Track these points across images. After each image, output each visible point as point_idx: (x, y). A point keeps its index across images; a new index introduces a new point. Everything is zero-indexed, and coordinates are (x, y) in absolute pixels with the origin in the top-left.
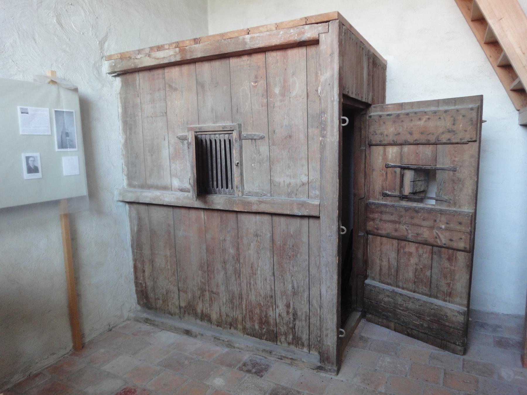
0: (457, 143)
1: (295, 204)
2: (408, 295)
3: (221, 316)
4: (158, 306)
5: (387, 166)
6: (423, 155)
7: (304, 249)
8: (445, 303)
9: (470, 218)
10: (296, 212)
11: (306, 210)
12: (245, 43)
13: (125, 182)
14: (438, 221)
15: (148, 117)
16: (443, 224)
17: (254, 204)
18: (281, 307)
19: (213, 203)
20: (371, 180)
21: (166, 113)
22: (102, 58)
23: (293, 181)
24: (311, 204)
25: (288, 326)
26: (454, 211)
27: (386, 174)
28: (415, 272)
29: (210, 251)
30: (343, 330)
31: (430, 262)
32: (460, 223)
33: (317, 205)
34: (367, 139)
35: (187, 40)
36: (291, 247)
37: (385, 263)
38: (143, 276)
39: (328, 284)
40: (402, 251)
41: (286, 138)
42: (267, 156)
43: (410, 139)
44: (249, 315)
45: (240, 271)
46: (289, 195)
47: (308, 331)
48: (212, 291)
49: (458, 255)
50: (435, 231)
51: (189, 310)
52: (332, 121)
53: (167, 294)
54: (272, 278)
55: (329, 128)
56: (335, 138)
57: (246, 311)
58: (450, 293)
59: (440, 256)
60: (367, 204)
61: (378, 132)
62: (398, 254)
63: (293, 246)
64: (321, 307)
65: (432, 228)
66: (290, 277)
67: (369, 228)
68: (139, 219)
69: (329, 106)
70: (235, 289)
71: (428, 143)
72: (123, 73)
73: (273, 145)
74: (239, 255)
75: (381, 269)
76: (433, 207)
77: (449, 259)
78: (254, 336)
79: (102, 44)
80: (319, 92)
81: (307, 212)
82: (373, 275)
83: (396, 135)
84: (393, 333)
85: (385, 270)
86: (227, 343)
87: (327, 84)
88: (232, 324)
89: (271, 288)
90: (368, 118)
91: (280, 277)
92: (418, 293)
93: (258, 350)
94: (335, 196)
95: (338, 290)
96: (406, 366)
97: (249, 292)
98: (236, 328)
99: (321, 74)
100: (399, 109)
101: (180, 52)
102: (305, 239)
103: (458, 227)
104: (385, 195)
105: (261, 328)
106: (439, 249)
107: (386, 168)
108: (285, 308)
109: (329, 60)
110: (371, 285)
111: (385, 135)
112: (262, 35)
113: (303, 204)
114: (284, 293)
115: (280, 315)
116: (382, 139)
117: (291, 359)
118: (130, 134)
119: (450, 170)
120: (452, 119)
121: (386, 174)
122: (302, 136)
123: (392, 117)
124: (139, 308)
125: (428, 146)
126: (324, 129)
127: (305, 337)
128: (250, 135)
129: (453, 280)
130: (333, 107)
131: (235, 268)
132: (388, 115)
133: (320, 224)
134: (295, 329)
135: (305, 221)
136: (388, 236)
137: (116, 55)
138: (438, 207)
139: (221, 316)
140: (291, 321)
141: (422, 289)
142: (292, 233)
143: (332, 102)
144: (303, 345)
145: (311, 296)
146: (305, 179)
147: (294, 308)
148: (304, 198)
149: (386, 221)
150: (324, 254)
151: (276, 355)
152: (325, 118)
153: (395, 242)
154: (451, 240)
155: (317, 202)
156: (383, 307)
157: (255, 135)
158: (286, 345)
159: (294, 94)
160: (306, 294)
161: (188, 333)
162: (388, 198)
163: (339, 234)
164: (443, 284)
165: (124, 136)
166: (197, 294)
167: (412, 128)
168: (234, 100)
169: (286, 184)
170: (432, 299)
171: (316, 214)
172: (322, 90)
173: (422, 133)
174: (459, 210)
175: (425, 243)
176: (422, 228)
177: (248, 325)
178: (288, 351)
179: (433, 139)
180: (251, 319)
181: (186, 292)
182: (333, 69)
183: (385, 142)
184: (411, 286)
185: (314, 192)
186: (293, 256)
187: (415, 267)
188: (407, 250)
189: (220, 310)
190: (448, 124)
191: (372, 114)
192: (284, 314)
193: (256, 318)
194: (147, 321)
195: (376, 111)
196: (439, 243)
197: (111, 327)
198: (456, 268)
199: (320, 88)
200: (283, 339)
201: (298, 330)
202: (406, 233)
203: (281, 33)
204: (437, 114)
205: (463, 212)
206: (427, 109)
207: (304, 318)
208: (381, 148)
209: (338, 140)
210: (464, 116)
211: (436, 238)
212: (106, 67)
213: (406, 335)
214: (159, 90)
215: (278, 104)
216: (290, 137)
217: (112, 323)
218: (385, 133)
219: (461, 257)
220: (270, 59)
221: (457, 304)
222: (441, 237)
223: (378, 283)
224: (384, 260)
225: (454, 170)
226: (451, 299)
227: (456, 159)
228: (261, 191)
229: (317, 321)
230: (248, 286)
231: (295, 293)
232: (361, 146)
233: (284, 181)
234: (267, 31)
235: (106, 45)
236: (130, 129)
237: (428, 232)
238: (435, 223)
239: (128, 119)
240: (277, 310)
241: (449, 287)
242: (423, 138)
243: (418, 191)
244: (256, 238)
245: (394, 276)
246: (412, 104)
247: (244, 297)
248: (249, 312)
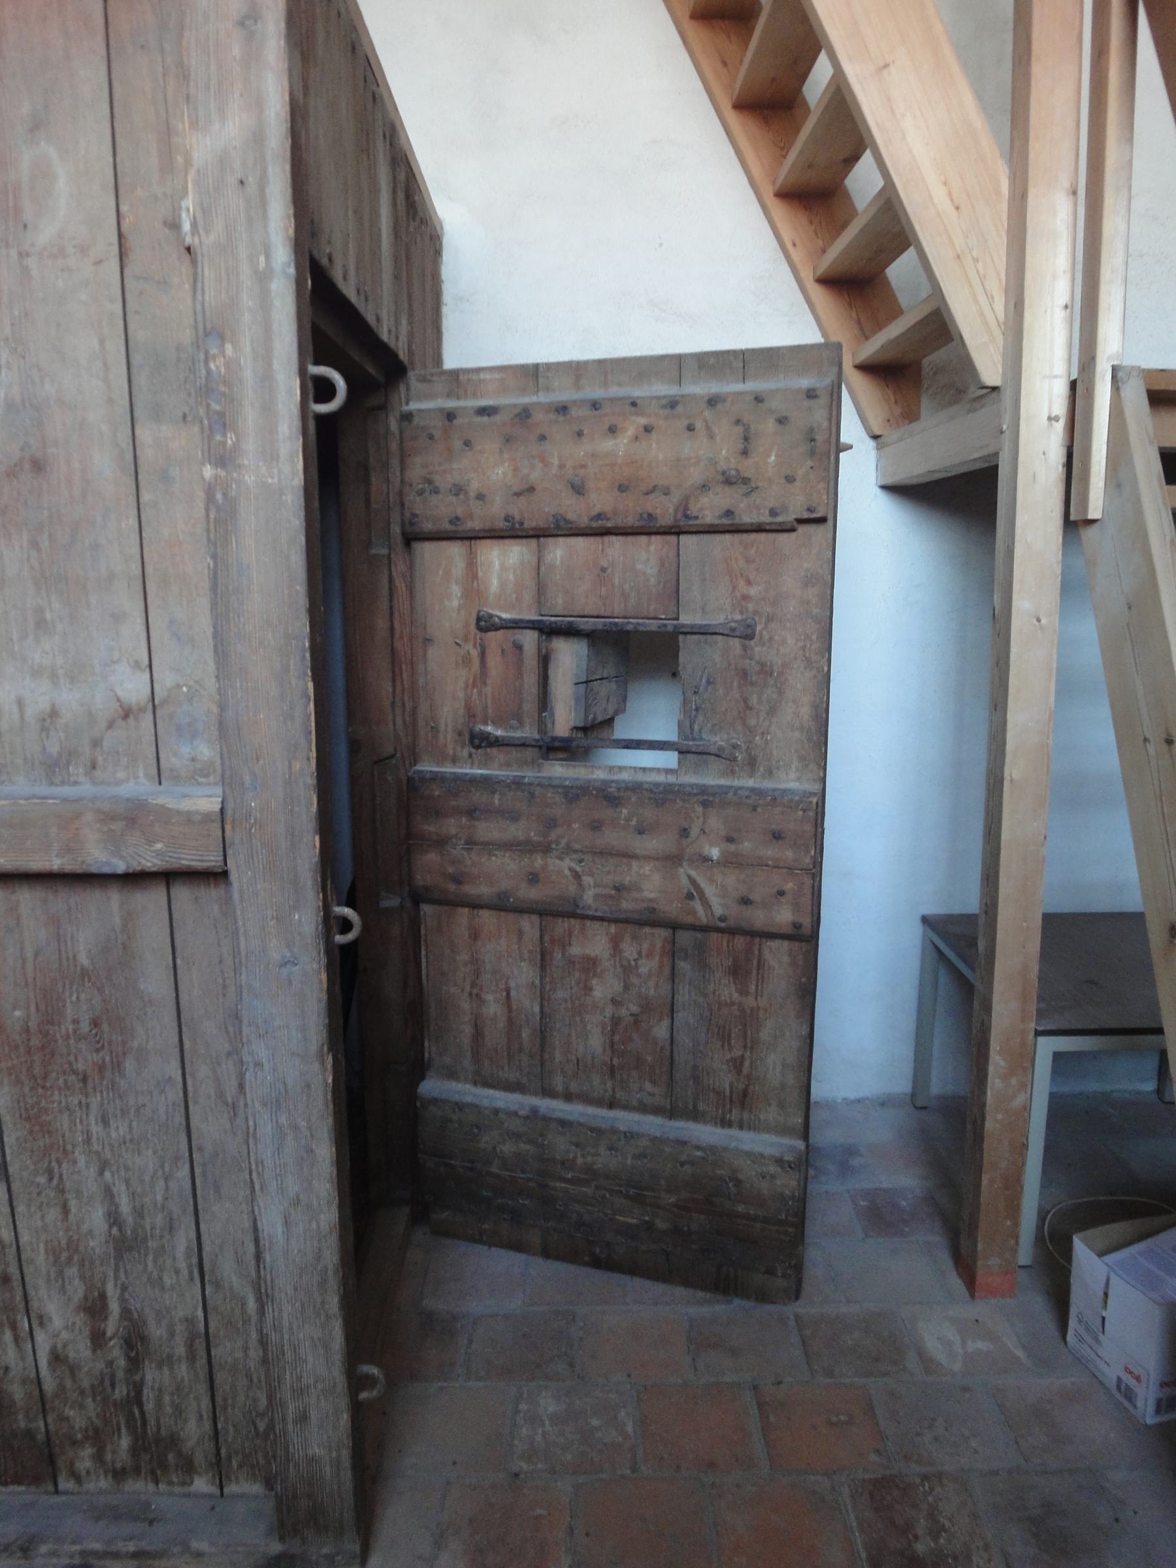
0: (759, 529)
1: (89, 817)
5: (485, 624)
6: (626, 577)
7: (156, 1032)
8: (727, 1131)
9: (811, 814)
10: (98, 856)
11: (150, 842)
14: (694, 832)
16: (712, 845)
18: (57, 1322)
20: (421, 681)
23: (69, 699)
24: (178, 812)
26: (753, 790)
27: (483, 655)
28: (613, 1032)
30: (374, 1371)
31: (666, 988)
32: (777, 836)
33: (206, 818)
34: (396, 517)
36: (85, 1027)
37: (493, 1007)
39: (293, 1186)
40: (558, 955)
43: (577, 510)
47: (205, 1402)
49: (767, 955)
50: (685, 871)
52: (266, 379)
55: (250, 417)
56: (286, 468)
58: (745, 1093)
59: (703, 965)
60: (410, 780)
61: (444, 482)
62: (543, 968)
63: (95, 1023)
64: (263, 1298)
65: (672, 860)
66: (93, 1171)
67: (421, 879)
69: (247, 301)
71: (647, 529)
75: (478, 1034)
76: (671, 779)
77: (738, 972)
80: (186, 226)
81: (158, 854)
82: (447, 1059)
83: (518, 494)
84: (541, 1268)
85: (495, 1035)
87: (232, 180)
90: (393, 425)
91: (42, 1180)
92: (626, 1107)
94: (297, 766)
95: (341, 1207)
96: (622, 1414)
99: (194, 124)
100: (523, 391)
103: (770, 852)
104: (481, 742)
106: (699, 935)
107: (480, 629)
108: (80, 1319)
109: (237, 51)
110: (445, 1101)
111: (472, 494)
113: (133, 817)
114: (67, 1253)
116: (460, 512)
119: (730, 634)
120: (739, 429)
121: (483, 655)
122: (105, 466)
123: (498, 418)
125: (643, 539)
126: (223, 422)
127: (193, 1431)
129: (751, 1044)
132: (483, 411)
133: (228, 901)
134: (140, 1405)
135: (152, 899)
136: (502, 905)
138: (689, 779)
140: (120, 1374)
141: (641, 1090)
142: (84, 960)
143: (263, 278)
144: (188, 1468)
145: (207, 1248)
146: (132, 686)
147: (126, 1312)
148: (135, 785)
149: (489, 847)
150: (263, 1054)
152: (228, 365)
153: (529, 925)
154: (745, 901)
155: (206, 801)
156: (498, 1177)
158: (104, 1483)
160: (183, 1240)
162: (494, 751)
163: (330, 948)
164: (717, 1062)
167: (583, 466)
169: (30, 712)
170: (681, 1124)
171: (211, 860)
172: (205, 210)
173: (622, 488)
174: (767, 784)
175: (650, 919)
176: (635, 864)
178: (115, 1514)
179: (665, 510)
182: (258, 104)
183: (475, 525)
184: (599, 1084)
185: (185, 750)
186: (101, 1068)
187: (609, 1011)
188: (575, 950)
190: (725, 452)
191: (413, 406)
192: (81, 1350)
195: (431, 396)
196: (702, 915)
198: (763, 1002)
199: (189, 203)
200: (85, 1459)
202: (572, 889)
204: (680, 409)
205: (785, 791)
206: (637, 392)
207: (181, 1351)
208: (455, 550)
209: (299, 480)
210: (782, 421)
211: (690, 896)
213: (586, 1264)
216: (38, 466)
218: (475, 486)
219: (778, 956)
221: (768, 1129)
222: (710, 891)
223: (469, 1087)
224: (489, 997)
225: (747, 634)
226: (746, 1116)
227: (753, 591)
229: (246, 1349)
231: (126, 1243)
232: (369, 544)
233: (20, 703)
237: (656, 877)
238: (684, 842)
240: (40, 1337)
241: (739, 1072)
242: (629, 510)
243: (600, 719)
245: (531, 1056)
246: (577, 370)
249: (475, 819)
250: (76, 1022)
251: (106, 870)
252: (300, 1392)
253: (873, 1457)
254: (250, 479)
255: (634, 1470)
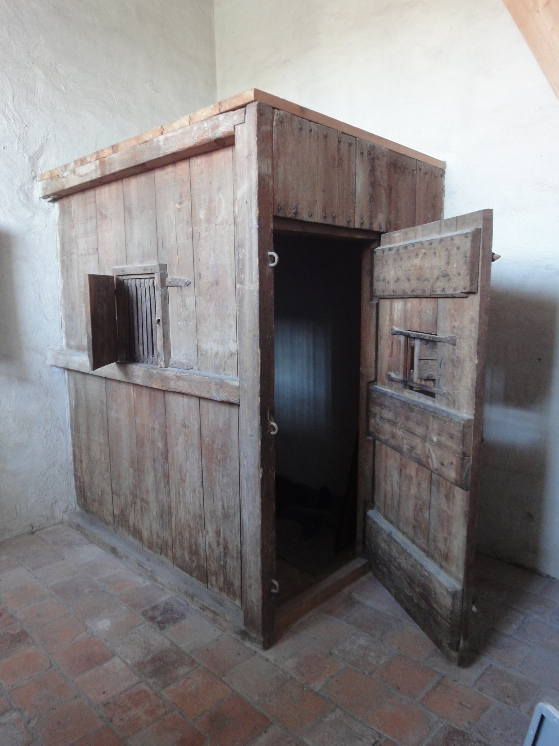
1: (213, 383)
2: (403, 546)
3: (151, 534)
4: (95, 510)
12: (159, 148)
13: (64, 341)
15: (82, 255)
17: (171, 379)
19: (133, 375)
21: (97, 249)
22: (35, 177)
24: (231, 385)
25: (219, 563)
29: (140, 442)
33: (236, 387)
35: (105, 149)
36: (220, 447)
38: (81, 468)
41: (212, 285)
42: (193, 311)
44: (179, 539)
45: (169, 474)
46: (217, 369)
48: (143, 499)
51: (121, 520)
52: (251, 258)
53: (102, 494)
54: (201, 490)
55: (247, 270)
56: (255, 285)
57: (176, 533)
63: (222, 446)
68: (77, 391)
70: (165, 500)
72: (59, 196)
73: (199, 295)
74: (167, 451)
78: (183, 569)
79: (34, 160)
86: (149, 573)
87: (245, 202)
88: (163, 548)
89: (200, 505)
91: (209, 490)
93: (180, 591)
97: (179, 506)
98: (166, 555)
101: (100, 164)
102: (234, 437)
105: (191, 559)
108: (215, 535)
112: (175, 134)
115: (210, 546)
117: (214, 612)
118: (67, 277)
124: (78, 509)
128: (176, 280)
130: (251, 237)
131: (164, 470)
137: (47, 174)
139: (151, 534)
140: (222, 557)
143: (251, 229)
147: (224, 538)
151: (197, 601)
157: (180, 280)
158: (217, 590)
159: (220, 219)
161: (114, 551)
165: (62, 281)
166: (129, 500)
168: (160, 230)
171: (234, 399)
176: (416, 437)
177: (178, 553)
180: (181, 544)
181: (118, 495)
189: (151, 526)
192: (214, 545)
193: (186, 544)
194: (78, 527)
197: (34, 529)
201: (230, 571)
203: (195, 128)
208: (388, 302)
212: (38, 191)
214: (91, 218)
215: (203, 234)
216: (217, 283)
217: (36, 525)
220: (195, 168)
228: (187, 361)
230: (177, 496)
231: (226, 516)
234: (181, 128)
235: (41, 161)
236: (67, 271)
239: (65, 258)
244: (183, 430)
247: (174, 512)
248: (179, 534)
249: (382, 409)
250: (218, 444)
251: (215, 399)
252: (250, 577)
253: (466, 724)
254: (247, 288)
255: (370, 674)
